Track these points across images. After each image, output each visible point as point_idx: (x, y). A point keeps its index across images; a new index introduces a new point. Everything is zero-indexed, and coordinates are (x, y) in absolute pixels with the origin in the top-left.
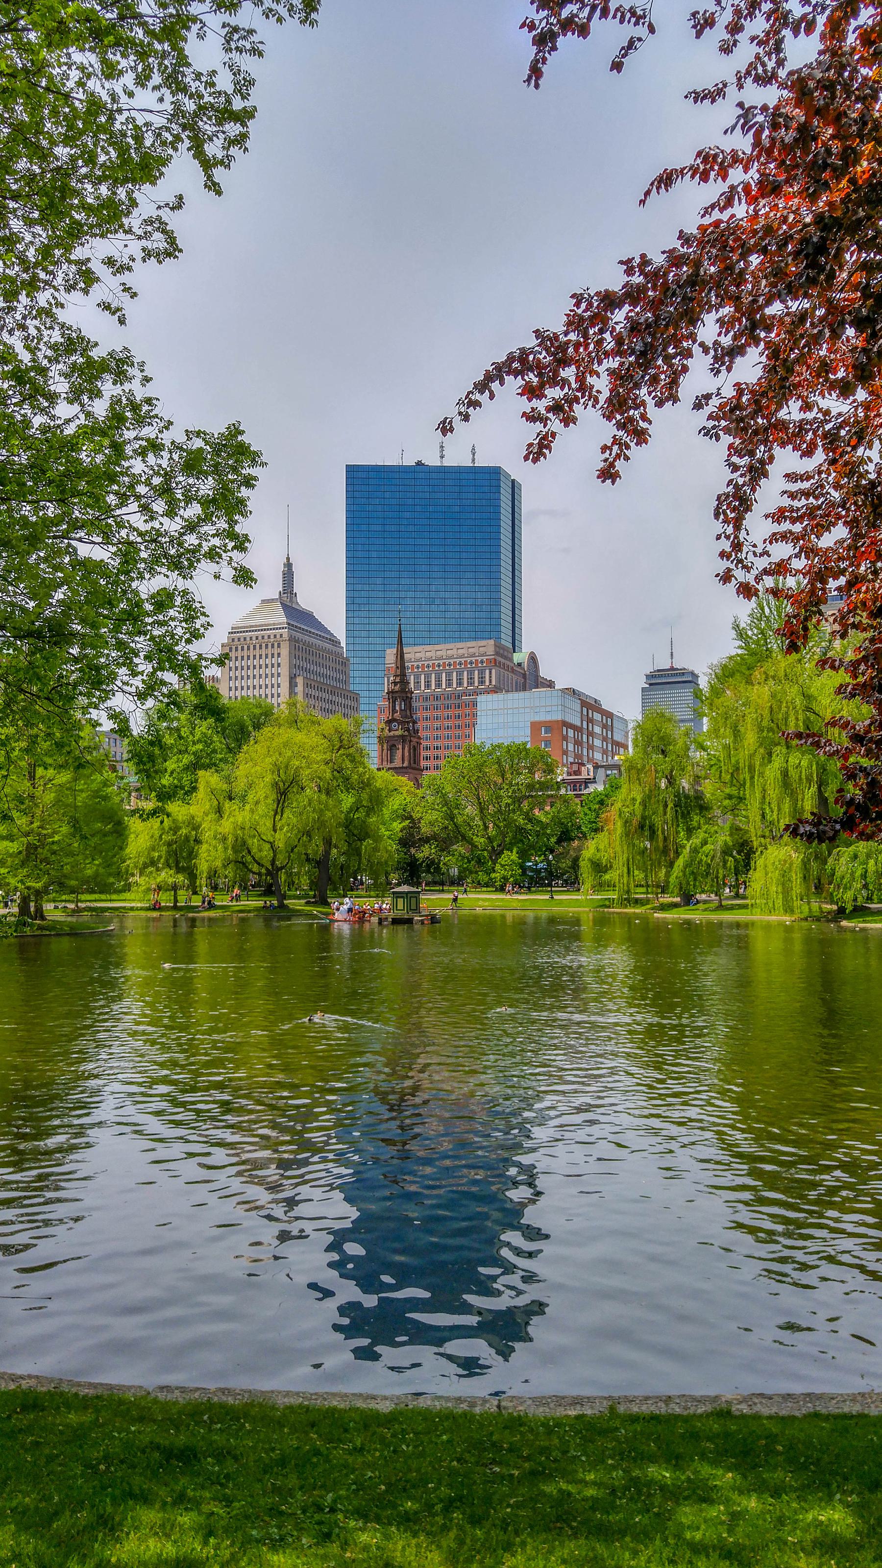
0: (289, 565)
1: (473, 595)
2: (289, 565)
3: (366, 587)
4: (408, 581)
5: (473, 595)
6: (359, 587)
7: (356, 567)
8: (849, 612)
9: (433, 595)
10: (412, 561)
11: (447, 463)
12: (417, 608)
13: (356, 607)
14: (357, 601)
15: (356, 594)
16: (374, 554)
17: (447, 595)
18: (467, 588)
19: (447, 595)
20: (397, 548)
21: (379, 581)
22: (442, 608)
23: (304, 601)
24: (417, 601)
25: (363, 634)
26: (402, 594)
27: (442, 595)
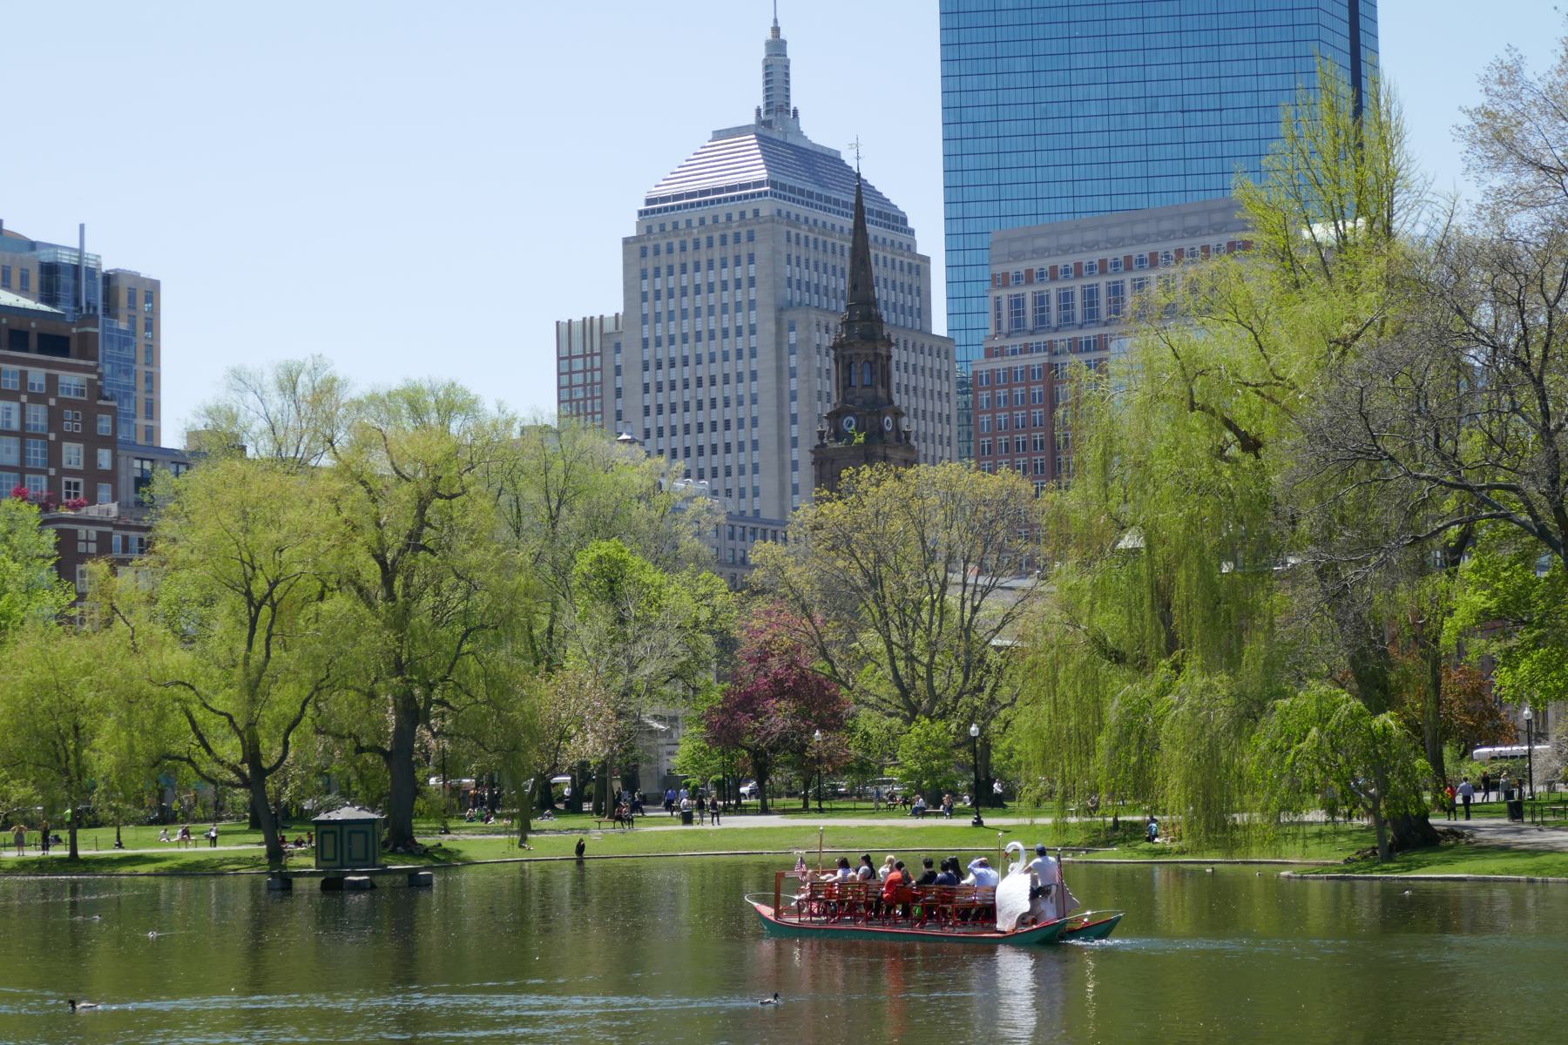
23: (818, 126)
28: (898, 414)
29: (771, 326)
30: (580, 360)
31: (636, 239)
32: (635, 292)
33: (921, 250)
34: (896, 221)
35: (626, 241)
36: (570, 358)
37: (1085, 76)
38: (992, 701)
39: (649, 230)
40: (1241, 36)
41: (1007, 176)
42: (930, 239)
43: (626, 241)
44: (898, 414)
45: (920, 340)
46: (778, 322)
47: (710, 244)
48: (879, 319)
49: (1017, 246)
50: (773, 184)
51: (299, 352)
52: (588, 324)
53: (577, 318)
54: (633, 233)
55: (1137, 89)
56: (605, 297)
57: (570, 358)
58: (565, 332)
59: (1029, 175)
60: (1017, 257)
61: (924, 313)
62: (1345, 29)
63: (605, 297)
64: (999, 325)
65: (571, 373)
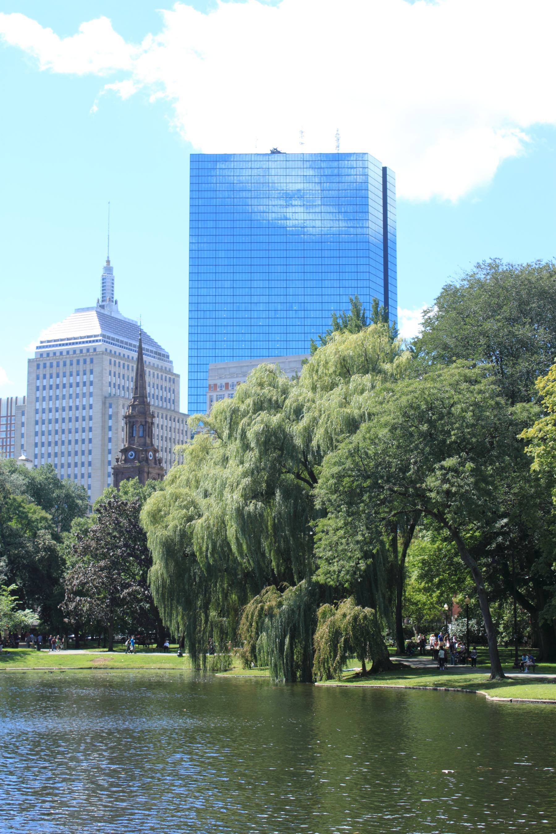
0: (108, 269)
1: (337, 299)
2: (108, 269)
3: (212, 291)
4: (261, 284)
5: (337, 299)
6: (203, 292)
7: (202, 269)
8: (513, 319)
9: (290, 299)
10: (265, 261)
11: (341, 151)
12: (272, 314)
13: (201, 314)
14: (202, 307)
15: (201, 299)
16: (222, 254)
17: (308, 299)
18: (330, 291)
19: (308, 299)
20: (354, 253)
21: (228, 284)
22: (301, 314)
23: (127, 309)
24: (272, 307)
25: (208, 345)
26: (255, 299)
27: (301, 299)
34: (163, 356)
35: (30, 361)
39: (41, 355)
41: (219, 337)
42: (180, 365)
43: (30, 361)
44: (156, 451)
45: (174, 415)
48: (149, 404)
50: (104, 336)
54: (33, 357)
61: (175, 402)
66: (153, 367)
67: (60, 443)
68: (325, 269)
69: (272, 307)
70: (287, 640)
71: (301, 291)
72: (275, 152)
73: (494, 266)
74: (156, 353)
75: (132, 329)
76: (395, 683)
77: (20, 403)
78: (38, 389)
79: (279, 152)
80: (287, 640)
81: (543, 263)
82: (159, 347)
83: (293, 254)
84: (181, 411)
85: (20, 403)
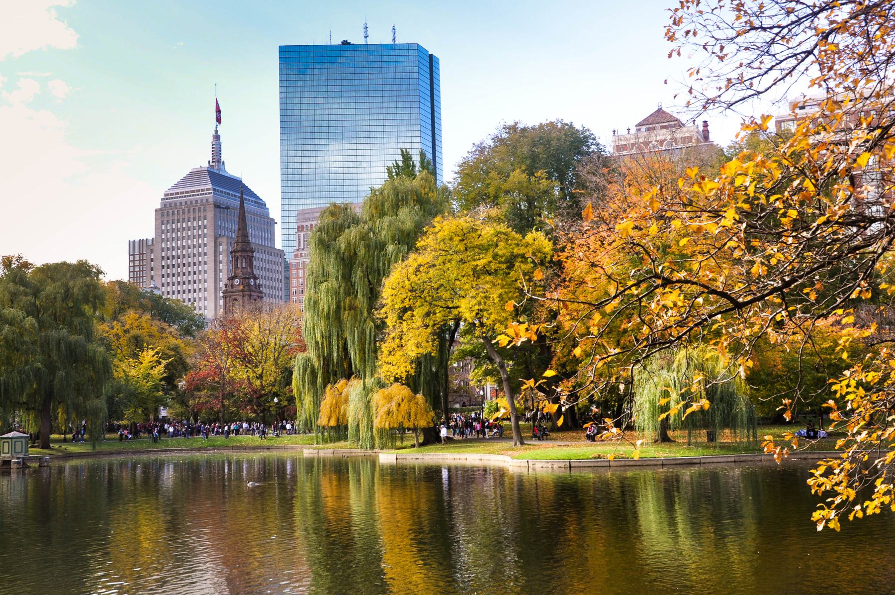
11: (370, 41)
23: (232, 169)
28: (255, 278)
29: (212, 244)
30: (872, 61)
31: (161, 209)
32: (159, 231)
33: (271, 216)
34: (261, 204)
35: (156, 210)
36: (134, 255)
37: (335, 153)
38: (788, 372)
39: (165, 205)
40: (392, 140)
41: (305, 189)
42: (275, 211)
43: (156, 210)
44: (255, 278)
45: (270, 250)
46: (215, 242)
47: (189, 212)
48: (249, 243)
49: (306, 216)
50: (214, 190)
51: (13, 253)
52: (141, 242)
53: (137, 239)
54: (159, 207)
55: (354, 158)
56: (147, 231)
57: (134, 255)
58: (132, 244)
59: (314, 189)
60: (307, 220)
61: (272, 240)
62: (430, 139)
63: (147, 231)
64: (299, 245)
65: (134, 261)
66: (253, 214)
67: (181, 274)
68: (386, 134)
69: (346, 165)
70: (226, 470)
71: (368, 152)
72: (345, 43)
73: (512, 129)
74: (255, 202)
75: (236, 185)
76: (457, 456)
77: (150, 243)
78: (163, 232)
79: (349, 44)
80: (226, 470)
81: (521, 126)
82: (258, 198)
83: (336, 123)
84: (276, 247)
85: (150, 243)
